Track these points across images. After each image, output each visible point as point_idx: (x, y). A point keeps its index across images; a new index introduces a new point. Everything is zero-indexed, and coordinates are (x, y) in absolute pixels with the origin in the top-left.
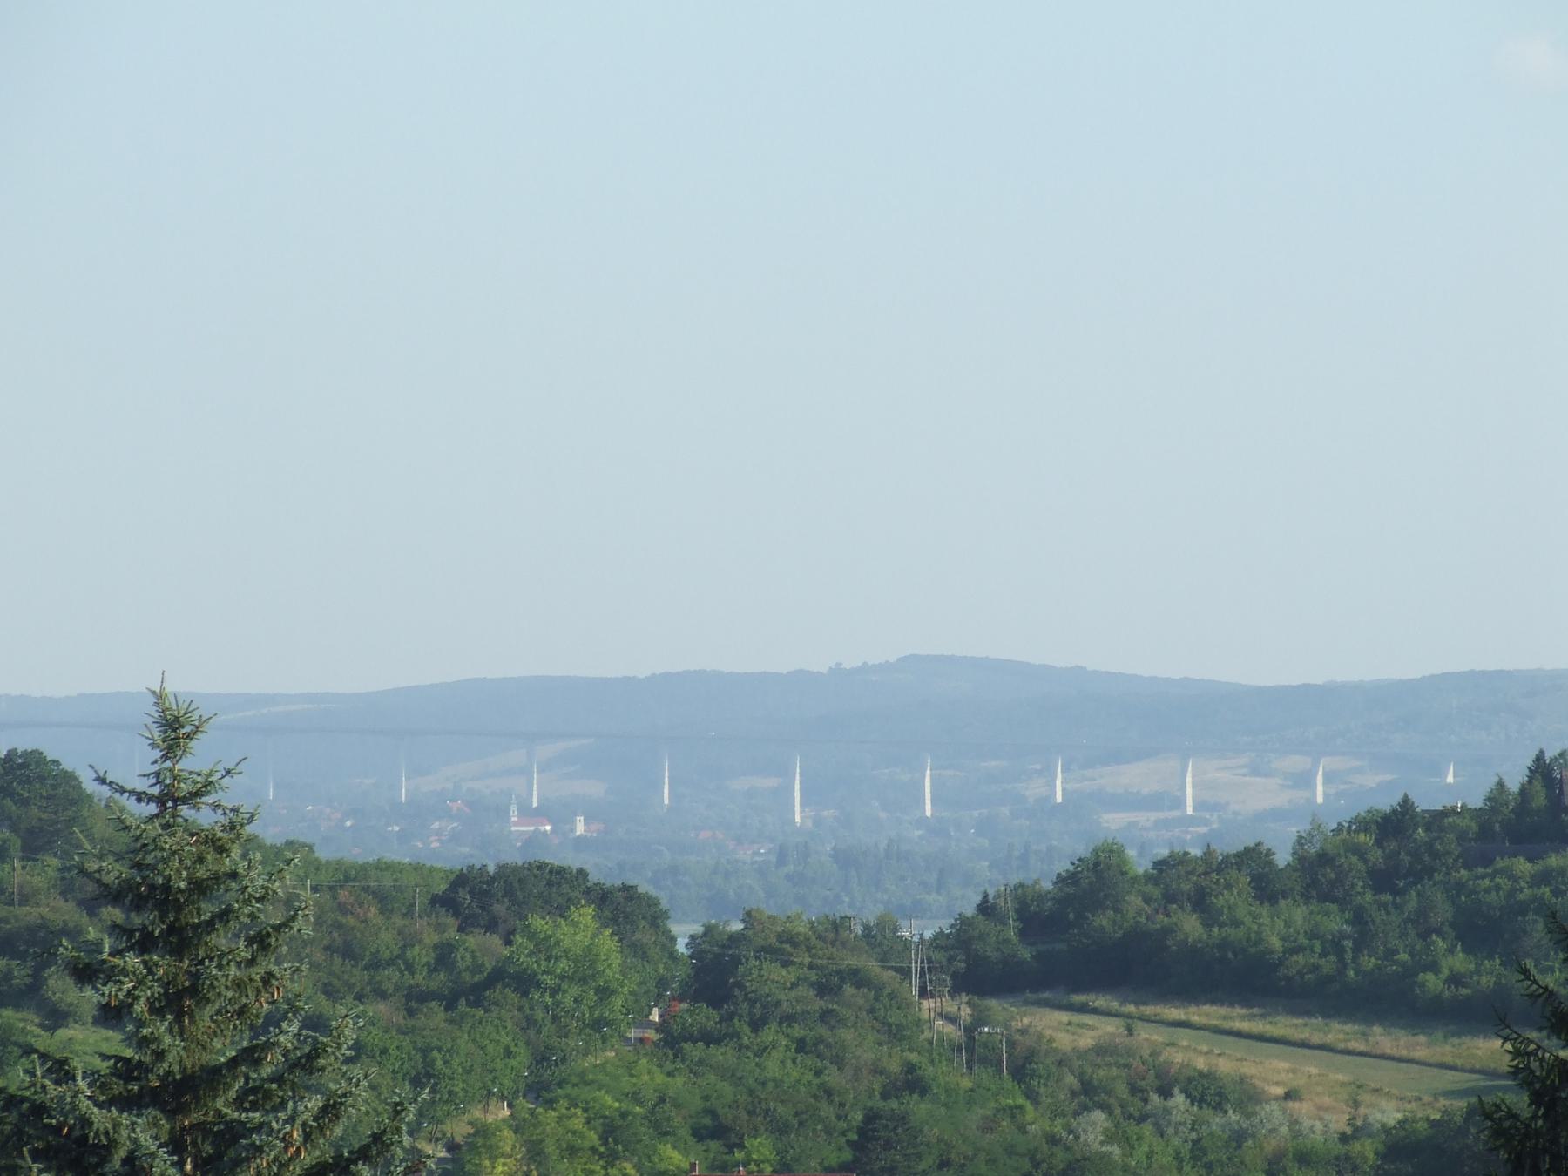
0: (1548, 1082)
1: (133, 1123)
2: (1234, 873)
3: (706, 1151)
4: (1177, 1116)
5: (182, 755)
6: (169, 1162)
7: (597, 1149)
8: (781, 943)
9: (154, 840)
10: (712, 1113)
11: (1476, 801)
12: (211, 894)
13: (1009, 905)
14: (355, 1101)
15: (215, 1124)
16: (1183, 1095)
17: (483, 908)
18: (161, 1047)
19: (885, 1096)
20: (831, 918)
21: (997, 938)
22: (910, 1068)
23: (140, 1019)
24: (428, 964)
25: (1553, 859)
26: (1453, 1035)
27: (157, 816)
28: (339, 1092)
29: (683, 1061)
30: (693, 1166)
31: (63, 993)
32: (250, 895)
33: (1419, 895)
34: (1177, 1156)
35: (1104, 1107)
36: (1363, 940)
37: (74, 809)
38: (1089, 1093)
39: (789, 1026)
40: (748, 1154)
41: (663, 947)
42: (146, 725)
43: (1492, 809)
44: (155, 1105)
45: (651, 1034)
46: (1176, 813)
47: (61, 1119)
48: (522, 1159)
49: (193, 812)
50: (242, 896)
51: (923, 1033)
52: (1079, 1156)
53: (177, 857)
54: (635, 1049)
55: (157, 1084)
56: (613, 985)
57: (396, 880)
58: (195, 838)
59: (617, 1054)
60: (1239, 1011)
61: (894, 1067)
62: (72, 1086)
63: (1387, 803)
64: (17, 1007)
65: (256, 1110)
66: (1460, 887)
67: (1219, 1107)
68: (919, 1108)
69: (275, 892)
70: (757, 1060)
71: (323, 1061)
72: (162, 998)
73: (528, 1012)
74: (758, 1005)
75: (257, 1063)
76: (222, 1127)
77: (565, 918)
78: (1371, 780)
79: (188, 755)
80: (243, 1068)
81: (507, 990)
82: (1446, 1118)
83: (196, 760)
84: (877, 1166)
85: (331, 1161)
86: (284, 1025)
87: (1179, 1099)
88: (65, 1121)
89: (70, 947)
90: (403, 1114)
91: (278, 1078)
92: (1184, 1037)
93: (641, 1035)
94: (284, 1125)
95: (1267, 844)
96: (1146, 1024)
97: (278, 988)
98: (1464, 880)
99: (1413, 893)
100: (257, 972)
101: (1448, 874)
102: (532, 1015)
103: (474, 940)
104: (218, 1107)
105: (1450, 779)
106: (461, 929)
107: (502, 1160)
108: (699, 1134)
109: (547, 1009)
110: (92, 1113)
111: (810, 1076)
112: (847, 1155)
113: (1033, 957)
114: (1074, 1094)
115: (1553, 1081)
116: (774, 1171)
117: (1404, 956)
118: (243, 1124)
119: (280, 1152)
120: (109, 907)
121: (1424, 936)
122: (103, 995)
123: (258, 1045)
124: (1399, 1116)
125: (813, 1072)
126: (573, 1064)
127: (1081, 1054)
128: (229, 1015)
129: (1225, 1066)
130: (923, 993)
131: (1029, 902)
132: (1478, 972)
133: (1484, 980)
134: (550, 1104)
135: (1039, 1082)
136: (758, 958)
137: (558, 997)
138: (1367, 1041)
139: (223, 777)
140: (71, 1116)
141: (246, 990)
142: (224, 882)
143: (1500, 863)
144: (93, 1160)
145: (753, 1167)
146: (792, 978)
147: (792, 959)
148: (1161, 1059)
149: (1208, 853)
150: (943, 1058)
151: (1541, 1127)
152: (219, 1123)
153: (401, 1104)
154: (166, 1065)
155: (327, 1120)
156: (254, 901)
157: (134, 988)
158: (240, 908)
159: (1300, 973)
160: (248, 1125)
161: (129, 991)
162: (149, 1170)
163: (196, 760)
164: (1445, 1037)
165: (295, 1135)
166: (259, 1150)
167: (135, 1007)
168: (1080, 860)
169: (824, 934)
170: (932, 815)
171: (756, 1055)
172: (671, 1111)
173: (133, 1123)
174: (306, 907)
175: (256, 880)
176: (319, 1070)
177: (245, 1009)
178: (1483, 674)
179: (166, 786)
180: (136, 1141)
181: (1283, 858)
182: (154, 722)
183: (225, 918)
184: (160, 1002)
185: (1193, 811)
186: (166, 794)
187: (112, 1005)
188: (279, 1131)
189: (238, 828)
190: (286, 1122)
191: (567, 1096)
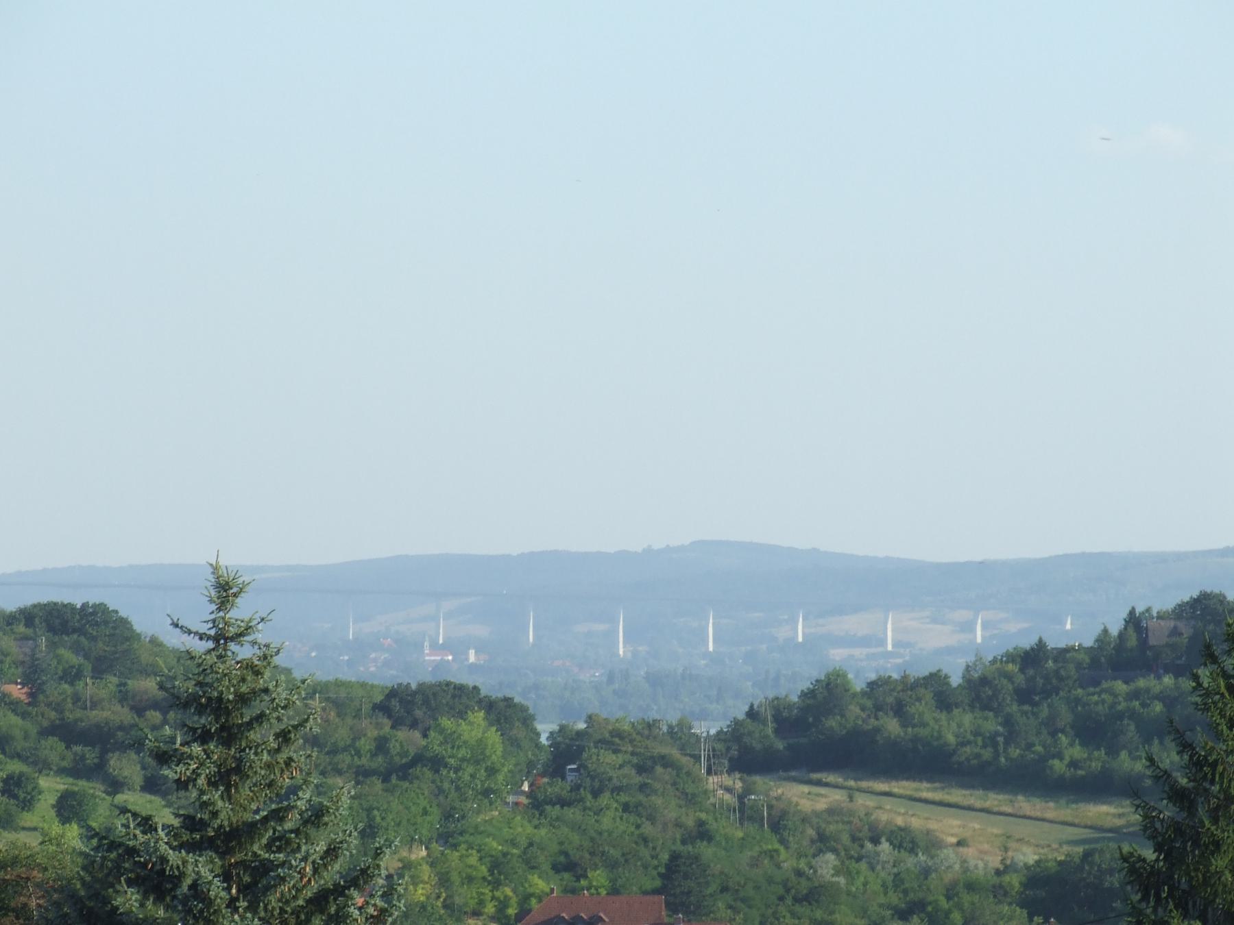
0: (1167, 837)
1: (196, 861)
2: (922, 690)
3: (561, 880)
4: (883, 857)
5: (231, 607)
6: (221, 888)
7: (486, 879)
8: (612, 737)
9: (211, 666)
10: (566, 854)
11: (1089, 642)
12: (250, 703)
13: (768, 712)
14: (348, 846)
15: (252, 862)
16: (888, 844)
17: (408, 713)
18: (216, 809)
19: (684, 842)
20: (646, 720)
21: (760, 733)
22: (701, 823)
23: (201, 790)
24: (370, 750)
25: (1141, 681)
26: (1073, 803)
27: (213, 649)
28: (338, 840)
29: (546, 818)
30: (552, 890)
31: (120, 770)
32: (277, 705)
33: (1049, 706)
34: (884, 885)
35: (835, 851)
36: (1012, 734)
37: (128, 643)
38: (823, 842)
39: (618, 794)
40: (590, 883)
41: (531, 739)
42: (206, 587)
43: (1099, 647)
44: (211, 848)
45: (523, 800)
46: (880, 649)
47: (147, 857)
48: (435, 885)
49: (238, 647)
50: (271, 706)
51: (709, 798)
52: (816, 884)
53: (227, 678)
54: (513, 810)
55: (213, 834)
56: (498, 766)
57: (348, 694)
58: (239, 665)
59: (500, 814)
60: (925, 785)
61: (690, 822)
62: (155, 835)
63: (1027, 643)
64: (88, 779)
65: (280, 853)
66: (1077, 700)
67: (912, 851)
68: (706, 851)
69: (294, 702)
70: (596, 817)
71: (326, 818)
72: (217, 774)
73: (439, 784)
74: (596, 780)
75: (281, 820)
76: (257, 864)
77: (465, 720)
78: (1013, 627)
79: (235, 608)
80: (272, 823)
81: (425, 768)
82: (1068, 859)
83: (241, 611)
84: (678, 891)
85: (332, 887)
86: (300, 794)
87: (885, 846)
88: (150, 860)
89: (153, 740)
90: (382, 856)
91: (297, 831)
92: (888, 803)
93: (515, 800)
94: (300, 862)
95: (945, 671)
96: (863, 794)
97: (296, 769)
98: (1080, 696)
99: (1045, 705)
100: (282, 757)
101: (1069, 691)
102: (442, 786)
103: (402, 734)
104: (255, 850)
105: (1068, 627)
106: (393, 727)
107: (421, 886)
108: (557, 868)
109: (452, 782)
110: (168, 854)
111: (632, 829)
112: (658, 883)
113: (784, 747)
114: (812, 842)
115: (1170, 836)
116: (608, 894)
117: (1039, 748)
118: (272, 862)
119: (297, 881)
120: (152, 711)
121: (1053, 734)
122: (176, 772)
123: (282, 808)
124: (1036, 857)
125: (634, 826)
126: (469, 820)
127: (817, 814)
128: (262, 787)
129: (916, 823)
130: (709, 772)
131: (782, 710)
132: (1090, 759)
133: (1094, 764)
134: (455, 847)
135: (789, 833)
136: (596, 747)
137: (460, 774)
138: (1013, 806)
139: (259, 623)
140: (154, 856)
141: (274, 769)
142: (259, 696)
143: (1105, 685)
144: (169, 886)
145: (593, 891)
146: (620, 761)
147: (619, 748)
148: (873, 817)
149: (905, 677)
150: (723, 816)
151: (1162, 867)
152: (255, 861)
153: (380, 848)
154: (219, 821)
155: (329, 859)
156: (280, 709)
157: (197, 768)
158: (270, 713)
159: (968, 759)
160: (275, 863)
161: (194, 770)
162: (207, 893)
163: (241, 611)
164: (1067, 804)
165: (308, 869)
166: (283, 880)
167: (198, 781)
168: (817, 681)
169: (641, 731)
170: (713, 650)
171: (595, 814)
172: (537, 852)
173: (196, 861)
174: (316, 713)
175: (282, 694)
176: (323, 825)
177: (273, 783)
178: (1091, 555)
179: (219, 629)
180: (198, 873)
181: (956, 680)
182: (212, 586)
183: (260, 720)
184: (215, 777)
185: (893, 648)
186: (219, 635)
187: (183, 779)
188: (297, 866)
189: (269, 658)
190: (301, 860)
191: (466, 842)
